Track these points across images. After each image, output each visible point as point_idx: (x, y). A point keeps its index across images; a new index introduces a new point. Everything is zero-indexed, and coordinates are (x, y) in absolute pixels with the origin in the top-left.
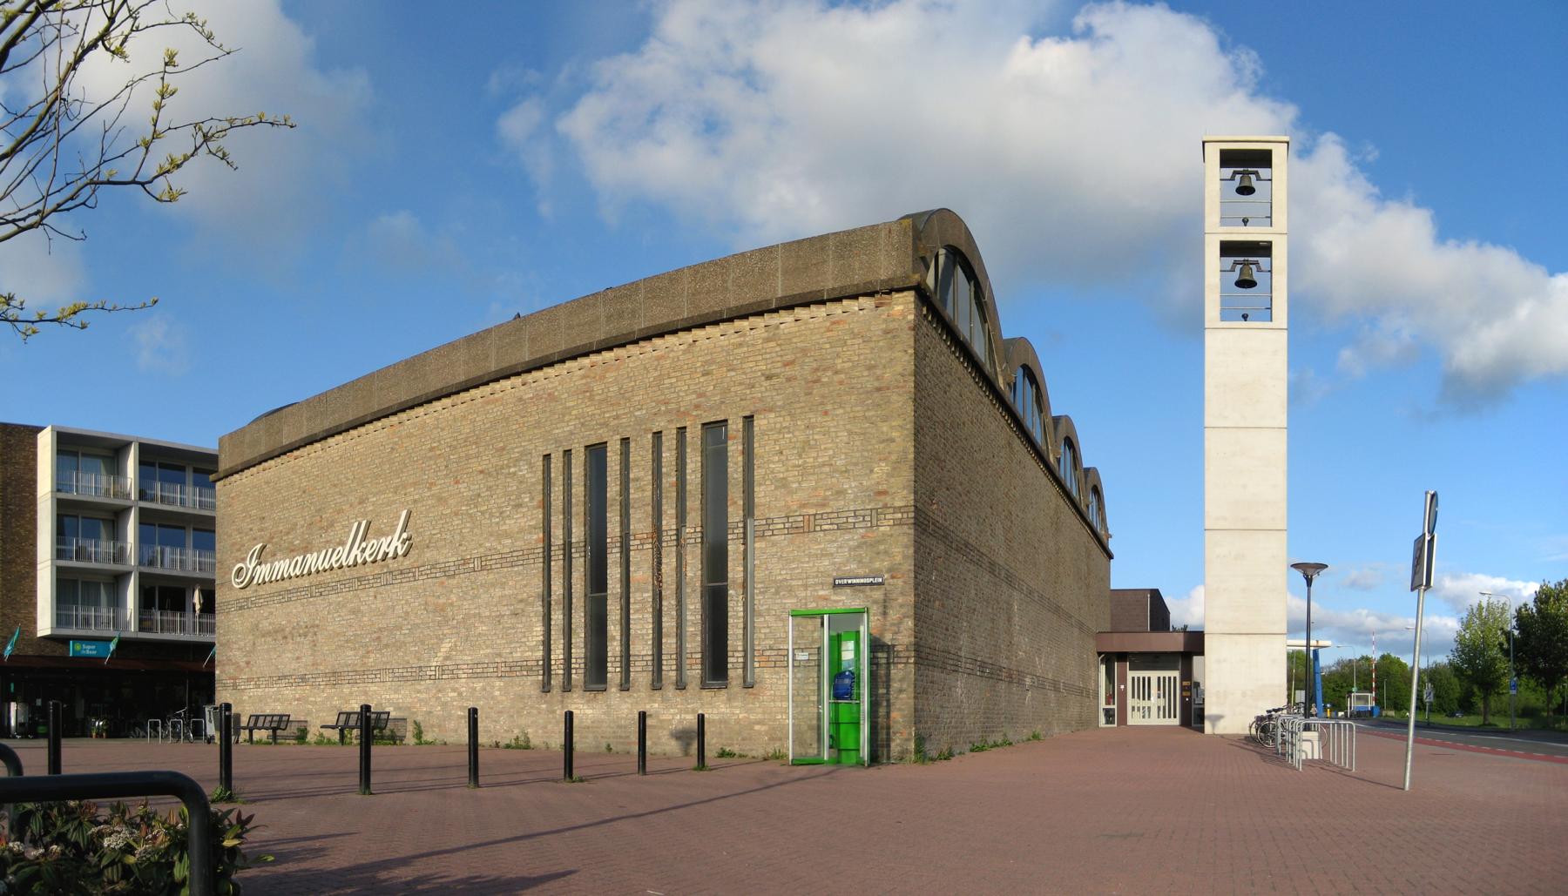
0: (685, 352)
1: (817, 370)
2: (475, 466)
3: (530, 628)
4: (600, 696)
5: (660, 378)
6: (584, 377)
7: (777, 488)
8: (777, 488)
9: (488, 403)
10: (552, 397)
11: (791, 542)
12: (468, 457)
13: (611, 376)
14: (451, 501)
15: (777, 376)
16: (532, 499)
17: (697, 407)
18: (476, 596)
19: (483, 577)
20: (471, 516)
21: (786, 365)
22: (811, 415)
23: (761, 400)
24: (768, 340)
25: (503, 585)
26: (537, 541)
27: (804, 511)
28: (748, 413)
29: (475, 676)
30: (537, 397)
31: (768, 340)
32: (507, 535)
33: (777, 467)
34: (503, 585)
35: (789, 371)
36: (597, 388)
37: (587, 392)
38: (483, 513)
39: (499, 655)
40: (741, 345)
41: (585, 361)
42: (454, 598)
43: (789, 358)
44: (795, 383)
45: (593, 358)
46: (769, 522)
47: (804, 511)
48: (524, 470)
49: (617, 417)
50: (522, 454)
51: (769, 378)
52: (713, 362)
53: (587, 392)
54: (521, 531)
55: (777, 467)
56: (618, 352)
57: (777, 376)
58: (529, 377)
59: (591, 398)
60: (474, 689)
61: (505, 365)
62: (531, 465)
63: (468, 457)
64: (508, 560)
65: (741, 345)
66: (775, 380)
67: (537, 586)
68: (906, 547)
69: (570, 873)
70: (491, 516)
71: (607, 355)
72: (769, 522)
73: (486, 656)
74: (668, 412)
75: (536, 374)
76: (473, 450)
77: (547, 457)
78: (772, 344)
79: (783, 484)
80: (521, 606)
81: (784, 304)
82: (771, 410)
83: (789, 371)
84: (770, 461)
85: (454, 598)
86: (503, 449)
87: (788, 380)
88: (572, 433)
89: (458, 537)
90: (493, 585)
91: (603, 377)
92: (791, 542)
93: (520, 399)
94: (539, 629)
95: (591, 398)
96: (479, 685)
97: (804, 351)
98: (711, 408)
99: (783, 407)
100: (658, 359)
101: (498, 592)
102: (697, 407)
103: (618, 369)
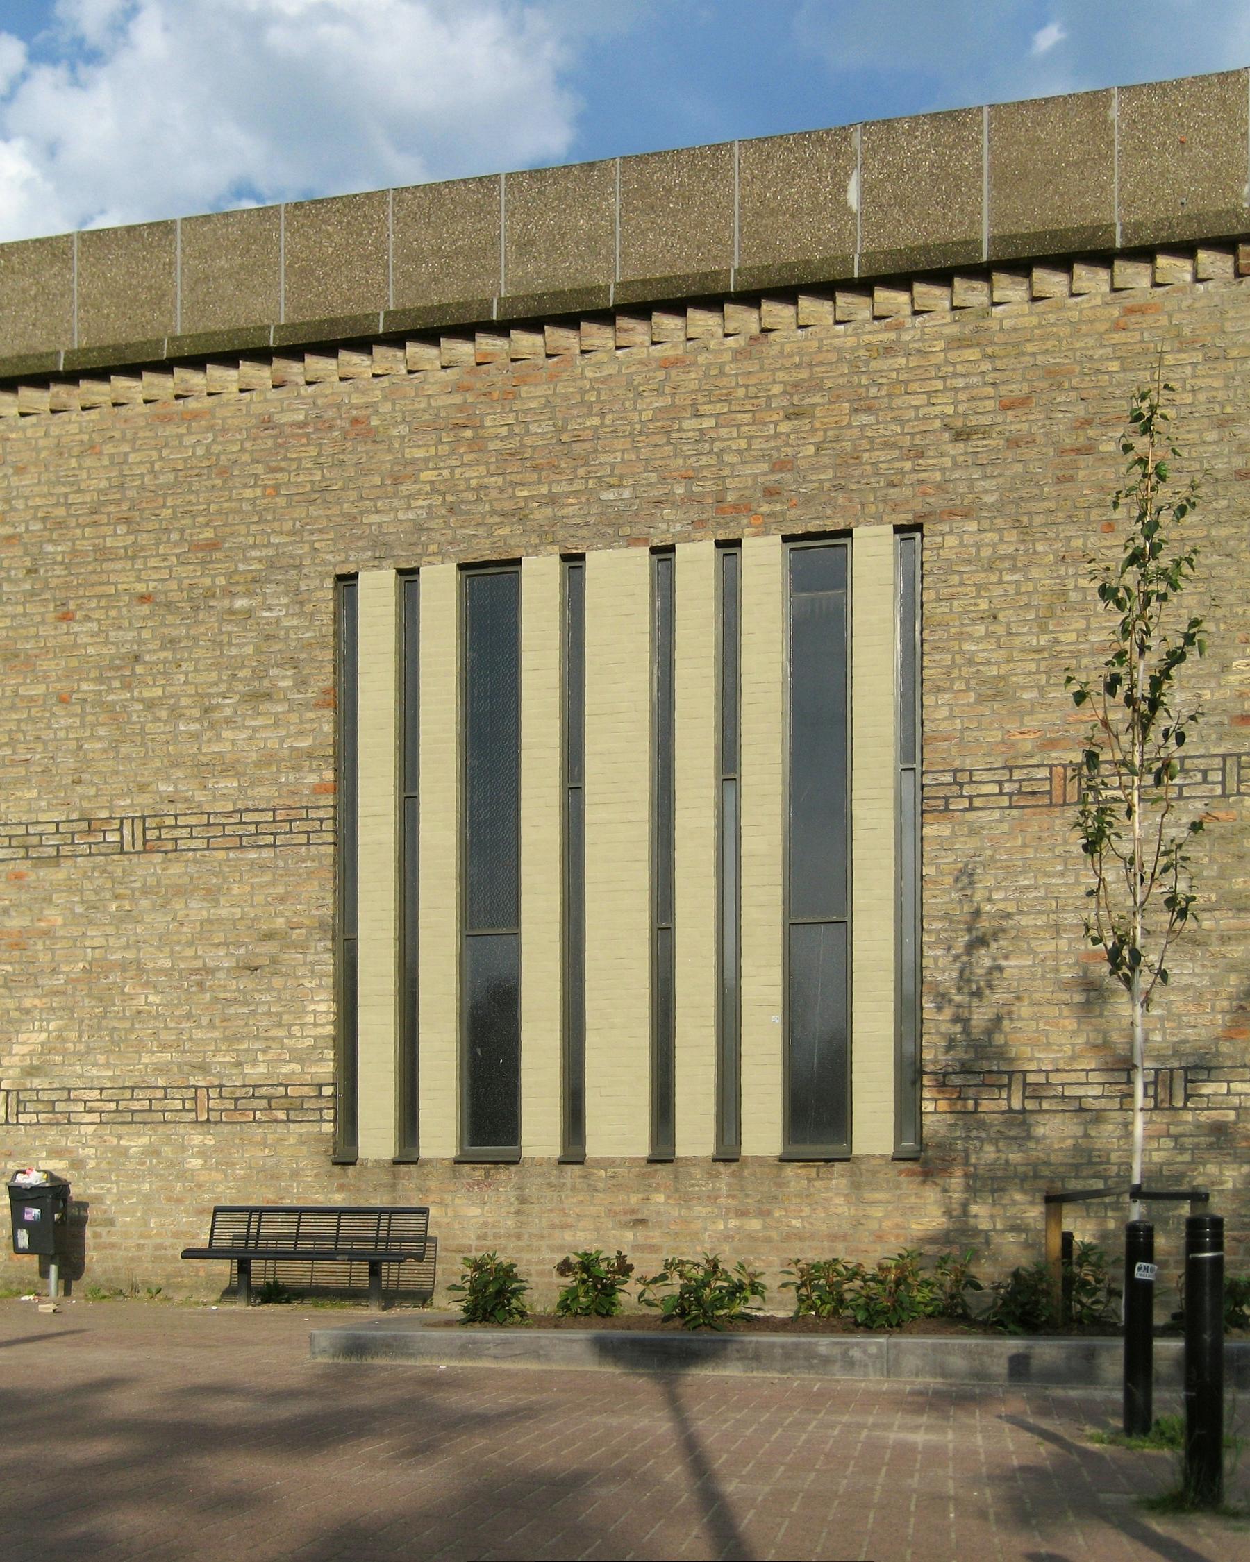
0: (738, 354)
1: (1087, 423)
2: (126, 580)
3: (296, 1003)
4: (502, 1173)
5: (672, 413)
6: (459, 388)
7: (980, 700)
8: (980, 700)
9: (166, 419)
10: (360, 429)
11: (1019, 828)
12: (103, 555)
13: (533, 395)
14: (45, 665)
15: (986, 432)
16: (301, 683)
17: (771, 493)
18: (124, 917)
19: (149, 868)
20: (109, 708)
21: (1006, 406)
22: (1070, 531)
23: (940, 487)
24: (959, 343)
25: (212, 895)
26: (318, 790)
27: (1053, 756)
28: (906, 519)
29: (123, 1118)
30: (320, 423)
31: (959, 343)
32: (225, 767)
33: (983, 650)
34: (212, 895)
35: (1014, 423)
36: (495, 423)
37: (463, 428)
38: (150, 705)
39: (203, 1068)
40: (888, 350)
41: (461, 350)
42: (54, 916)
43: (1017, 389)
44: (1028, 452)
45: (487, 343)
46: (962, 779)
47: (1053, 756)
48: (277, 609)
49: (550, 500)
50: (271, 564)
51: (961, 435)
52: (817, 386)
53: (463, 428)
54: (268, 759)
55: (983, 650)
56: (558, 337)
57: (986, 432)
58: (293, 370)
59: (477, 444)
60: (125, 1152)
61: (1029, 225)
62: (299, 599)
63: (103, 555)
64: (233, 832)
65: (888, 350)
66: (978, 443)
67: (317, 898)
68: (326, 692)
69: (83, 1331)
70: (176, 714)
71: (524, 341)
72: (962, 779)
73: (158, 1070)
74: (692, 499)
75: (316, 364)
76: (119, 538)
77: (347, 581)
78: (973, 354)
79: (997, 691)
80: (270, 948)
81: (521, 311)
82: (966, 515)
83: (1014, 423)
84: (961, 636)
85: (54, 916)
86: (213, 546)
87: (1014, 443)
88: (420, 528)
89: (68, 762)
90: (181, 891)
91: (511, 395)
92: (1019, 828)
93: (267, 423)
94: (323, 1006)
95: (477, 444)
96: (137, 1142)
97: (1054, 376)
98: (808, 500)
99: (999, 507)
100: (666, 364)
101: (197, 909)
102: (771, 493)
103: (553, 378)
